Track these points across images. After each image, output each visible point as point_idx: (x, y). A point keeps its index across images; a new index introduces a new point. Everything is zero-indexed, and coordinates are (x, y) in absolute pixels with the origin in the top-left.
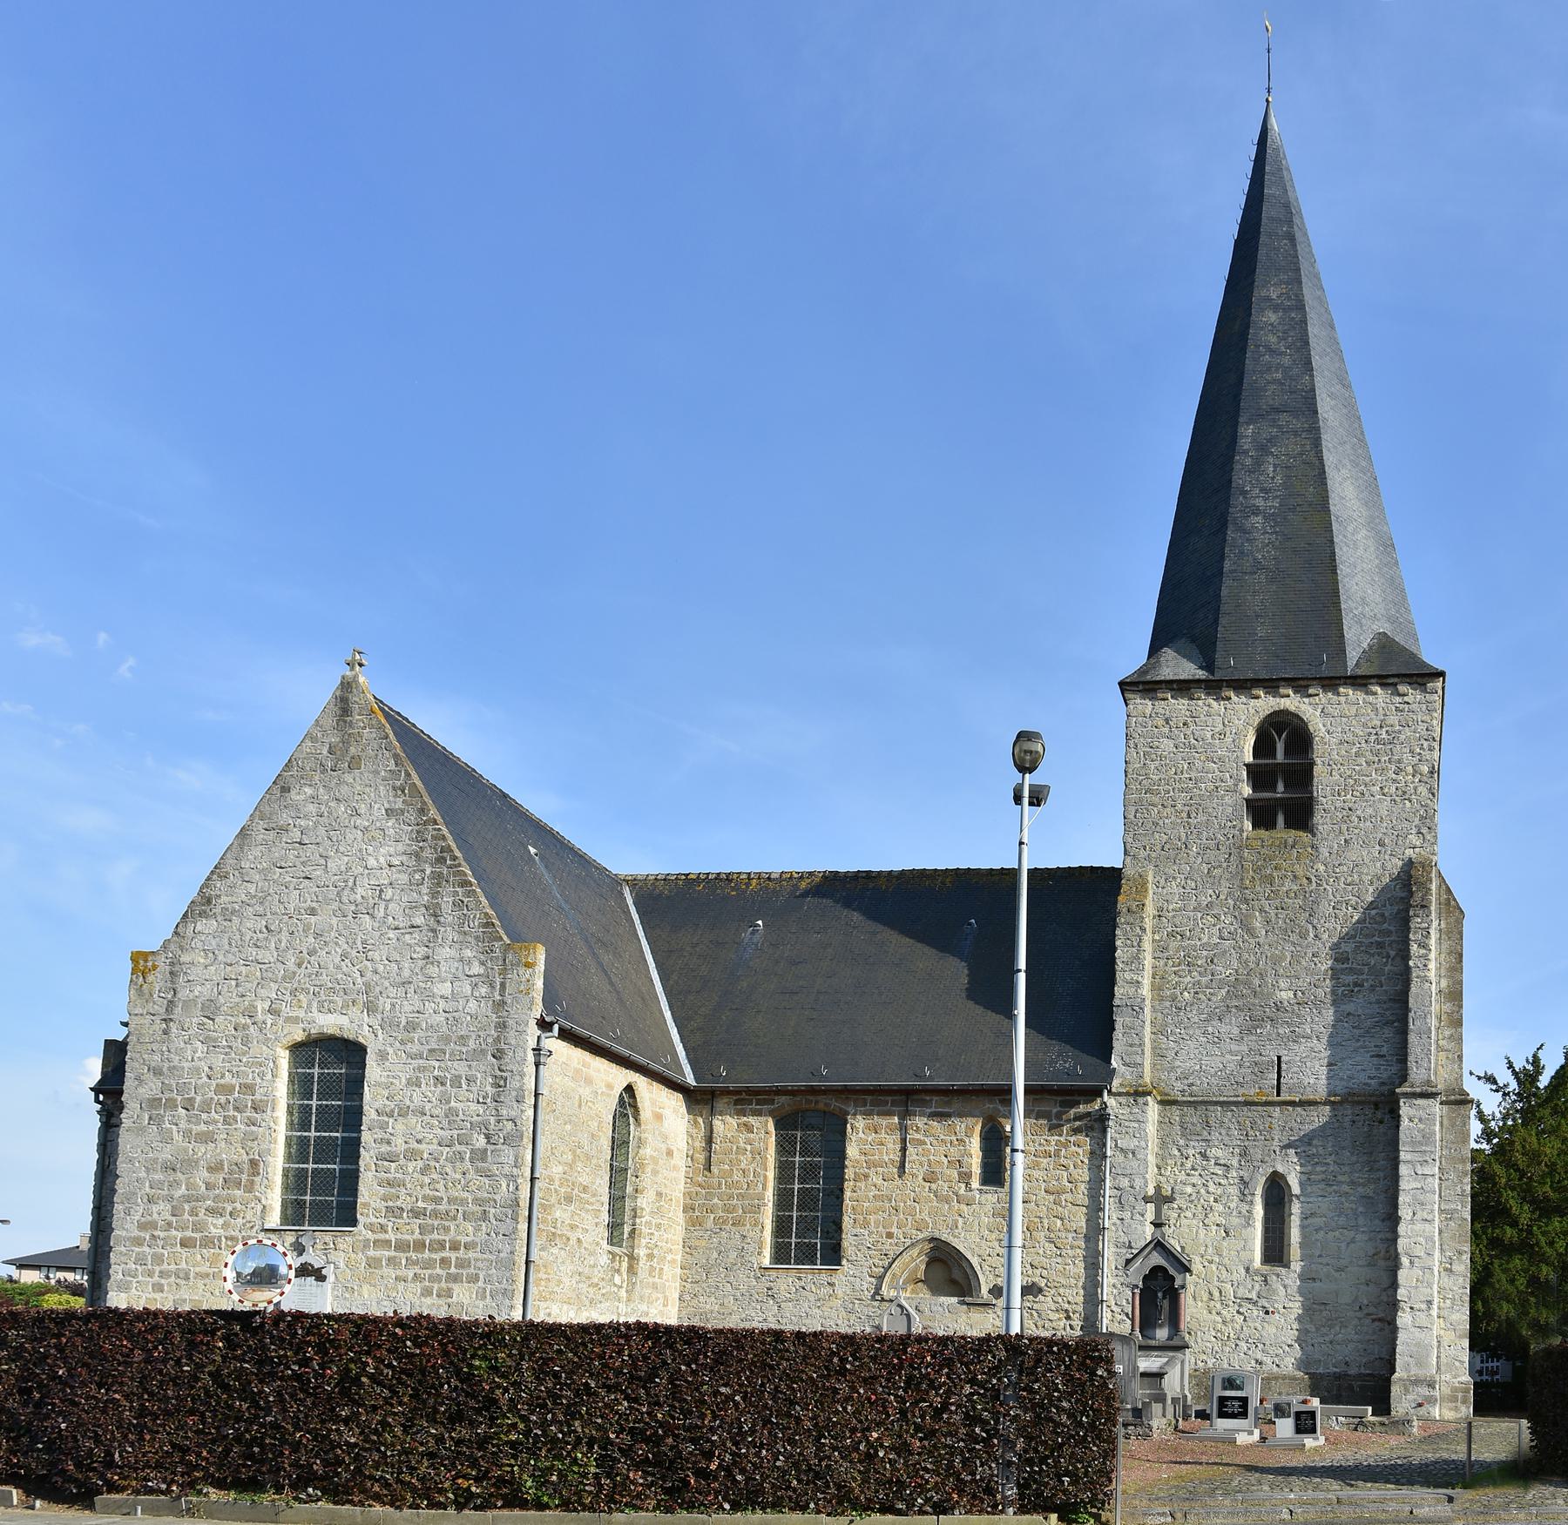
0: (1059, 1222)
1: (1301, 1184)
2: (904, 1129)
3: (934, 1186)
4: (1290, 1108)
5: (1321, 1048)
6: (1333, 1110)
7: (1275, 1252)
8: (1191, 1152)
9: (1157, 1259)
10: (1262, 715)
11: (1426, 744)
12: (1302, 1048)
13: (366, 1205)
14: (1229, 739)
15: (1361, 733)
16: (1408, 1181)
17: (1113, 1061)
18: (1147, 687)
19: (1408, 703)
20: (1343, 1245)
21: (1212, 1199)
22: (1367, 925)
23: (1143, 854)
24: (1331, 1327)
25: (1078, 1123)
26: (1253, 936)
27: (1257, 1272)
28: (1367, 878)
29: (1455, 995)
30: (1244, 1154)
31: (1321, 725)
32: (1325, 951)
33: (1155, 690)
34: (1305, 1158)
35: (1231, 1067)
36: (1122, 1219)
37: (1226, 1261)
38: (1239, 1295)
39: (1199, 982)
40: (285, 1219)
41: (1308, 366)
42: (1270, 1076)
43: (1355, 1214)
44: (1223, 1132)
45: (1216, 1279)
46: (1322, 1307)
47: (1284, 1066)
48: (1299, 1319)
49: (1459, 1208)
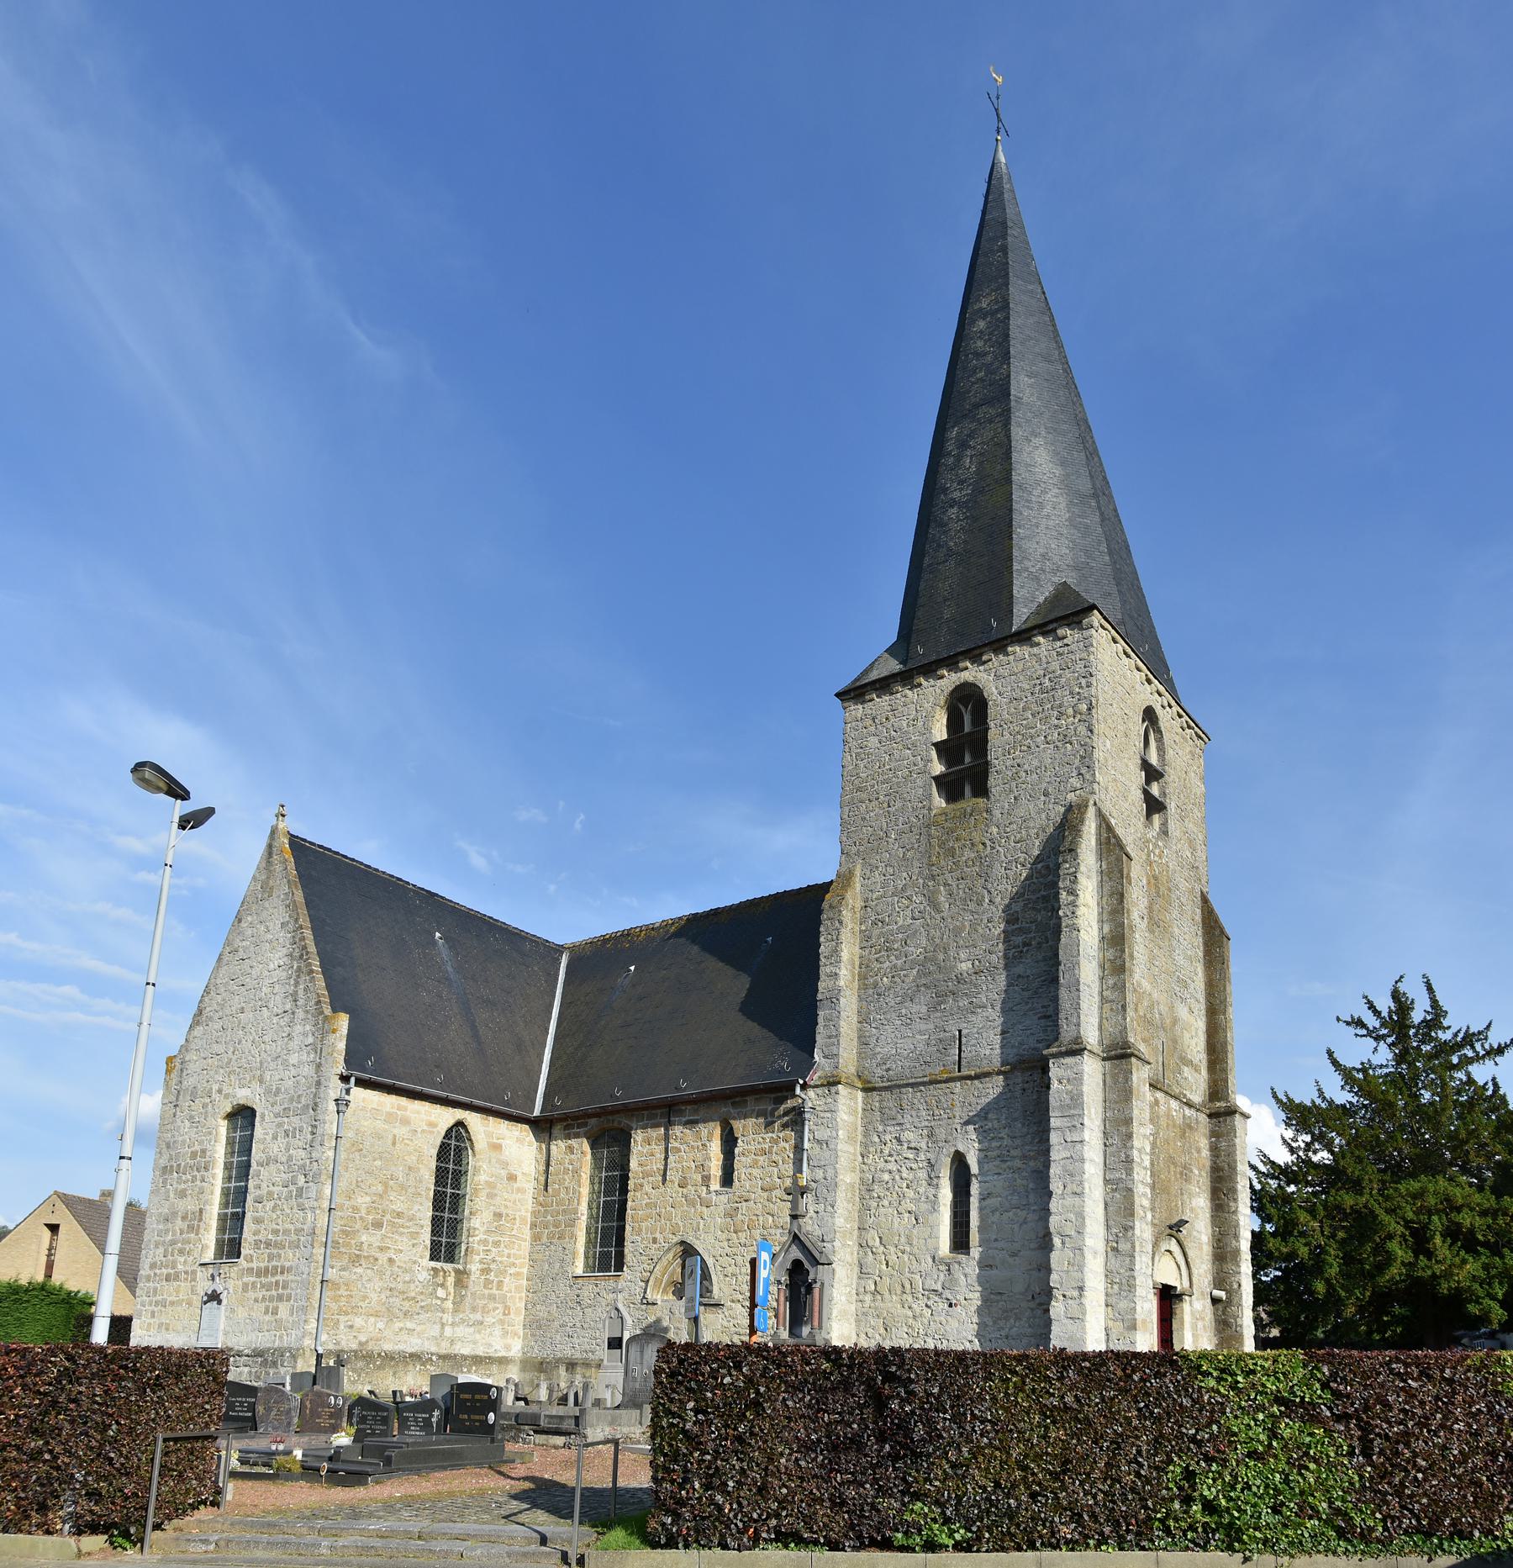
0: (770, 1218)
1: (979, 1163)
2: (667, 1138)
3: (685, 1190)
4: (969, 1082)
5: (995, 1016)
6: (1006, 1079)
7: (960, 1242)
8: (888, 1137)
9: (796, 1253)
10: (947, 691)
11: (1083, 682)
12: (978, 1020)
13: (246, 1239)
14: (920, 724)
15: (1028, 687)
16: (1059, 1151)
17: (816, 1055)
18: (857, 693)
19: (1068, 645)
20: (1016, 1227)
21: (905, 1185)
22: (1035, 880)
23: (854, 849)
24: (1007, 1319)
25: (786, 1118)
26: (939, 911)
27: (942, 1261)
28: (1033, 832)
29: (1116, 940)
30: (931, 1135)
31: (994, 689)
32: (998, 913)
33: (863, 694)
34: (983, 1133)
35: (921, 1047)
36: (817, 1212)
37: (915, 1250)
38: (926, 1287)
39: (895, 966)
40: (219, 1253)
41: (1006, 357)
42: (952, 1052)
43: (1027, 1191)
44: (914, 1114)
45: (907, 1270)
46: (999, 1297)
47: (964, 1040)
48: (979, 1311)
49: (1124, 1177)
